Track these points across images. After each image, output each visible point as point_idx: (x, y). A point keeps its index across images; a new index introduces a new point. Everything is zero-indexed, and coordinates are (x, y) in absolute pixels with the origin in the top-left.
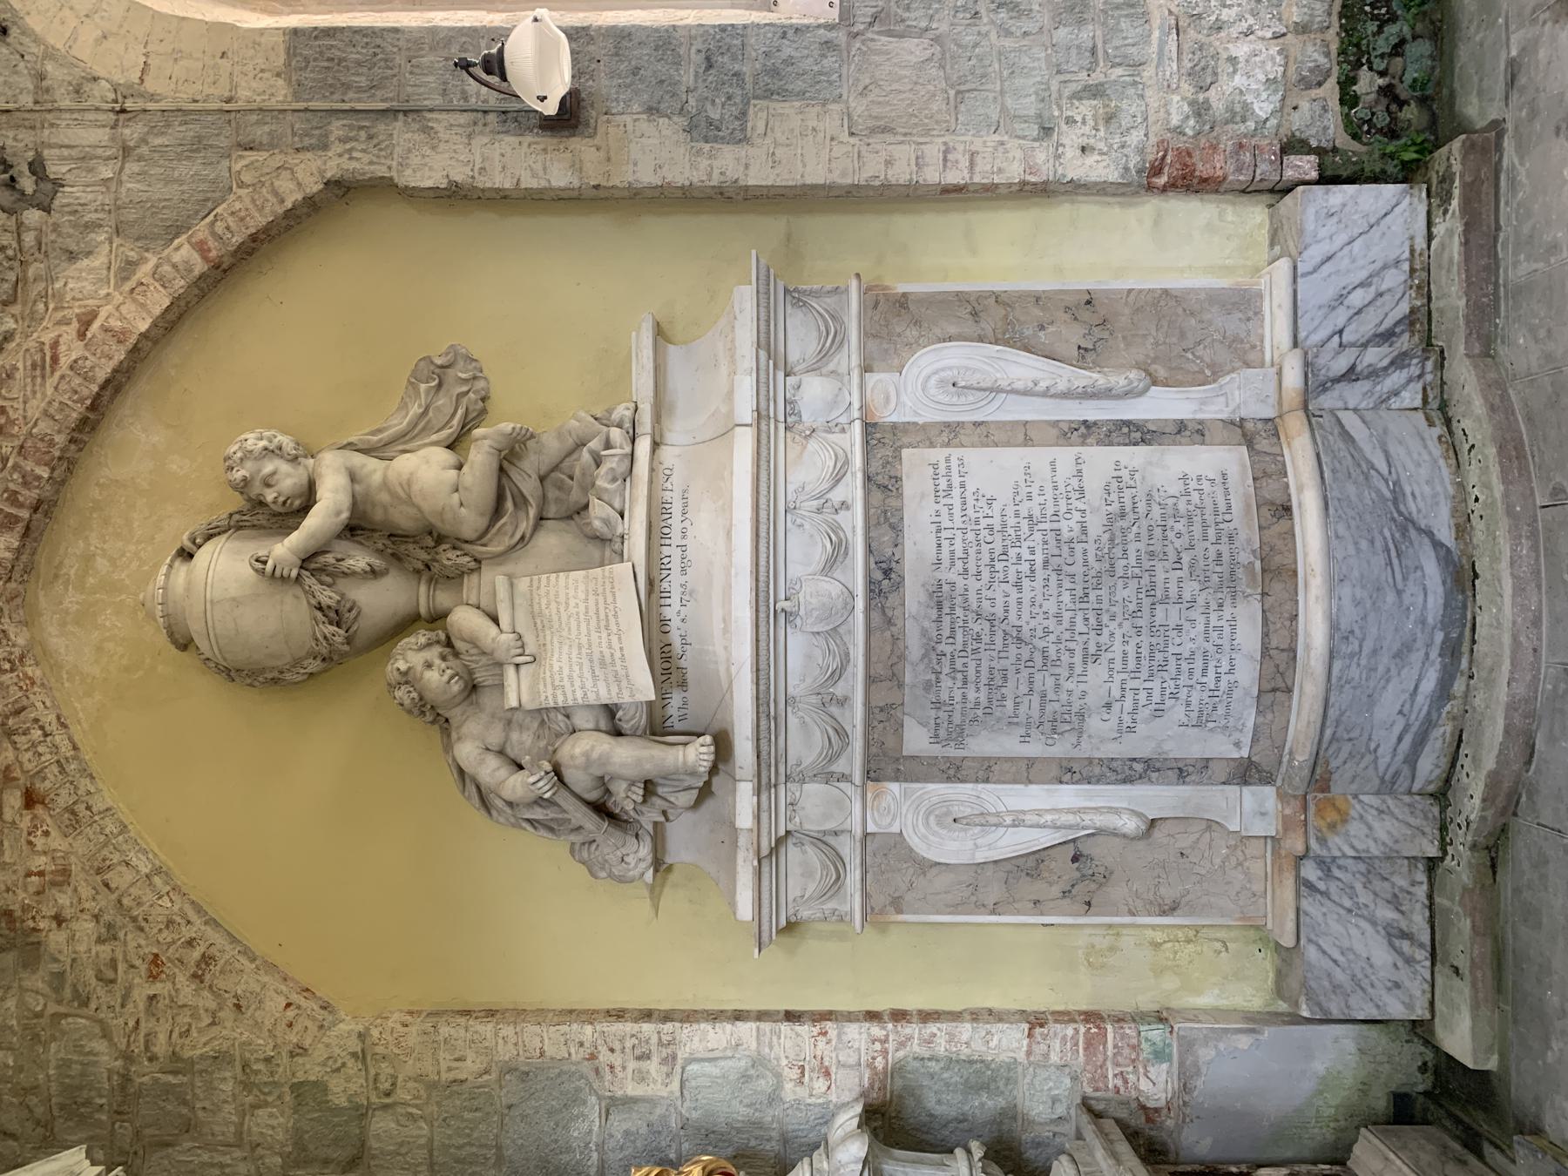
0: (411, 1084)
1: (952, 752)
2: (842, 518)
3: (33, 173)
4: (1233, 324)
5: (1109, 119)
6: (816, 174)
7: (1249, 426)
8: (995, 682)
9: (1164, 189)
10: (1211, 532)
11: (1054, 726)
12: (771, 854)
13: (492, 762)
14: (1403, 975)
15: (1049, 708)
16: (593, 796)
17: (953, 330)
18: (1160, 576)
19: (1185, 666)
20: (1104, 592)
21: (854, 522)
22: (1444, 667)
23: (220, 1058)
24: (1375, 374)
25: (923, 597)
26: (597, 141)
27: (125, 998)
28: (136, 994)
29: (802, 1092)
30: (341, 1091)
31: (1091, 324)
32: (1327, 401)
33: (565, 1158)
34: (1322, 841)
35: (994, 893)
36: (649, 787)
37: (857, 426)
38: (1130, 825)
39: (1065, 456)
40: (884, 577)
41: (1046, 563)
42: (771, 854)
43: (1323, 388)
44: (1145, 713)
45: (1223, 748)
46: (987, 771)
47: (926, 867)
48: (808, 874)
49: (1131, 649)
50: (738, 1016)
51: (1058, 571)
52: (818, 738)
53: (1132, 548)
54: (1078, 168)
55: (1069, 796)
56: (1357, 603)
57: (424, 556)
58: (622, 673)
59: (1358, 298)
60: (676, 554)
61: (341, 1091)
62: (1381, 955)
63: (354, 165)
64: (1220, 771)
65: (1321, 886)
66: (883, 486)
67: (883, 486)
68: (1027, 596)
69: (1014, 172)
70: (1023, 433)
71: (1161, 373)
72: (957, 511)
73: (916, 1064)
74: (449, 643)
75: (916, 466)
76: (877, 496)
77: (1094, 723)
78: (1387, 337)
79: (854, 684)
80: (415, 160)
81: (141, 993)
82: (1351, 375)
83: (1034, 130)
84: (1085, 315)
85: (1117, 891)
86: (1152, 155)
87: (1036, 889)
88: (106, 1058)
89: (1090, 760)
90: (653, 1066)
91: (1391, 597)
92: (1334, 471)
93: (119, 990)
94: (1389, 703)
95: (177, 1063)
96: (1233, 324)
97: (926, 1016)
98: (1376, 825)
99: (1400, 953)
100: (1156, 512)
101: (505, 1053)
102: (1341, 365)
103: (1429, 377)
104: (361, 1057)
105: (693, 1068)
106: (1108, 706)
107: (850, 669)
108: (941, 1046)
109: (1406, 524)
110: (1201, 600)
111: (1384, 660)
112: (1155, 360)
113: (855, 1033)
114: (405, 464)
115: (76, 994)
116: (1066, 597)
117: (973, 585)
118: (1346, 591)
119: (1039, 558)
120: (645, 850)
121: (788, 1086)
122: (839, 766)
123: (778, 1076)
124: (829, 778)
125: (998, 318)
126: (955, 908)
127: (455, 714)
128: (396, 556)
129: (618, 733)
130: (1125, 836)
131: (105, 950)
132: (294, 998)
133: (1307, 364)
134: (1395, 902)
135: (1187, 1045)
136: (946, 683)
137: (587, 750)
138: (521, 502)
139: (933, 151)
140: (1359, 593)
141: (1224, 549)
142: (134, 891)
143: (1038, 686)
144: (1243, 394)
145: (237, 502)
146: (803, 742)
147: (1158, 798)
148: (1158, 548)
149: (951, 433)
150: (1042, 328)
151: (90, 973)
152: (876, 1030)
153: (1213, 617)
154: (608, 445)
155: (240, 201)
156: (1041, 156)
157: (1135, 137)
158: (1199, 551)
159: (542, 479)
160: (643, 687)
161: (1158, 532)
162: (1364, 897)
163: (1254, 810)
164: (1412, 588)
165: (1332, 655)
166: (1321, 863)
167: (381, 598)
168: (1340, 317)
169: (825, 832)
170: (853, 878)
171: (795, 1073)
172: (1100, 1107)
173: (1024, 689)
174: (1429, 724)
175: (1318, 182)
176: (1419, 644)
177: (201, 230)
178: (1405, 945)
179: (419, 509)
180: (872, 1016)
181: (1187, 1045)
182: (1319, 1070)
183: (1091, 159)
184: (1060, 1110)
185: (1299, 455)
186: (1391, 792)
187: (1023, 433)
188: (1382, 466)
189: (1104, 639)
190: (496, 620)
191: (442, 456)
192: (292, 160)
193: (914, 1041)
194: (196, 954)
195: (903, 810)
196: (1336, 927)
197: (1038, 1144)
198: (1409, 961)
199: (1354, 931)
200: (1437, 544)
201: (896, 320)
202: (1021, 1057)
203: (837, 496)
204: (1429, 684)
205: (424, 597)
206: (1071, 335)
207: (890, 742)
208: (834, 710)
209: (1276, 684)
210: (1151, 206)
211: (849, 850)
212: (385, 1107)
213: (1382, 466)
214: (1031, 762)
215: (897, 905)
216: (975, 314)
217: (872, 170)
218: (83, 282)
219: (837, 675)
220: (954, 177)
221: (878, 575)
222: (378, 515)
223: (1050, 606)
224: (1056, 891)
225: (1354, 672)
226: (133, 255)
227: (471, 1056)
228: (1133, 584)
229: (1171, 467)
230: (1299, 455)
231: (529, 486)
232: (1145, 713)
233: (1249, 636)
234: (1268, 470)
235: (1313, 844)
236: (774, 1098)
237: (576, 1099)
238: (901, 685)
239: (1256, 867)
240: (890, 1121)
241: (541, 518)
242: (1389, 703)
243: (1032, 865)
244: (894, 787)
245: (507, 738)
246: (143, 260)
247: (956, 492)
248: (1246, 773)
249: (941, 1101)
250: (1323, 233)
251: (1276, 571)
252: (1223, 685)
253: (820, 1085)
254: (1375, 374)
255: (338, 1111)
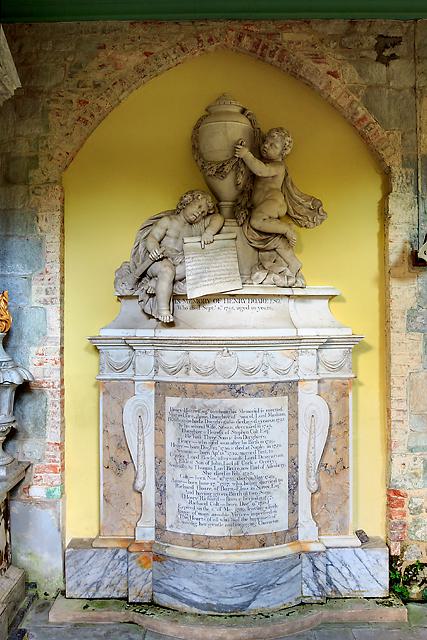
0: (36, 202)
1: (167, 416)
2: (261, 373)
3: (392, 55)
4: (335, 524)
5: (416, 474)
6: (395, 360)
7: (295, 531)
8: (196, 434)
9: (388, 496)
10: (255, 517)
11: (178, 456)
12: (126, 343)
13: (162, 232)
14: (82, 588)
15: (186, 455)
16: (149, 272)
17: (334, 416)
18: (238, 497)
19: (202, 506)
20: (231, 476)
21: (259, 377)
22: (203, 605)
23: (47, 128)
24: (316, 578)
25: (229, 406)
26: (407, 274)
27: (72, 92)
28: (74, 95)
29: (33, 354)
30: (34, 174)
31: (335, 468)
32: (305, 560)
33: (8, 262)
34: (134, 558)
35: (111, 430)
36: (152, 295)
37: (297, 378)
38: (139, 485)
39: (285, 460)
40: (236, 390)
41: (243, 454)
42: (126, 343)
43: (311, 559)
44: (183, 490)
45: (170, 520)
46: (160, 430)
47: (121, 404)
48: (118, 357)
49: (209, 486)
50: (62, 329)
51: (240, 458)
52: (172, 363)
53: (249, 486)
54: (397, 461)
55: (150, 461)
56: (227, 573)
57: (243, 203)
58: (198, 285)
59: (345, 571)
60: (245, 305)
61: (34, 174)
62: (90, 580)
63: (397, 177)
64: (160, 519)
65: (116, 557)
66: (274, 389)
67: (274, 389)
68: (230, 446)
69: (395, 438)
70: (293, 444)
71: (316, 496)
72: (264, 419)
73: (44, 399)
74: (209, 214)
75: (280, 402)
76: (269, 386)
77: (179, 471)
78: (330, 582)
79: (194, 377)
80: (399, 201)
81: (74, 97)
82: (315, 569)
83: (412, 445)
84: (340, 466)
85: (113, 478)
86: (402, 491)
87: (113, 444)
88: (48, 85)
89: (165, 469)
90: (43, 296)
91: (230, 585)
92: (278, 563)
93: (76, 89)
94: (189, 584)
95: (45, 112)
96: (335, 524)
97: (62, 403)
98: (141, 578)
99: (91, 586)
100: (263, 496)
101: (48, 238)
102: (319, 565)
103: (314, 598)
104: (48, 182)
105: (42, 312)
106: (186, 477)
107: (200, 376)
108: (51, 409)
109: (257, 590)
110: (228, 513)
111: (205, 583)
112: (322, 494)
113: (56, 376)
114: (281, 199)
115: (73, 73)
116: (229, 461)
117: (234, 425)
118: (232, 568)
119: (244, 451)
120: (127, 292)
121: (36, 349)
122: (160, 371)
123: (39, 345)
124: (156, 367)
125: (339, 426)
126: (105, 416)
127: (181, 217)
128: (242, 192)
129: (174, 282)
130: (135, 482)
131: (90, 83)
132: (71, 155)
133: (320, 553)
134: (110, 585)
135: (53, 505)
136: (195, 415)
137: (164, 271)
138: (265, 241)
139: (403, 406)
140: (232, 573)
141: (249, 521)
142: (112, 95)
143: (194, 450)
144: (307, 530)
145: (265, 130)
146: (171, 357)
147: (150, 495)
148: (249, 496)
149: (294, 415)
150: (335, 450)
151: (81, 78)
152: (57, 384)
153: (222, 518)
154: (288, 278)
155: (383, 134)
156: (402, 449)
157: (408, 485)
158: (249, 512)
159: (275, 250)
160: (194, 293)
161: (255, 497)
162: (112, 574)
163: (146, 533)
164: (234, 593)
165: (207, 563)
166: (124, 558)
167: (227, 187)
168: (338, 565)
169: (134, 364)
170: (117, 375)
171: (40, 352)
172: (29, 470)
173: (193, 445)
174: (180, 599)
175: (390, 555)
176: (211, 596)
177: (371, 118)
178: (94, 589)
179: (262, 203)
180: (62, 381)
181: (53, 505)
182: (42, 560)
183: (401, 468)
184: (28, 455)
185: (285, 550)
186: (153, 584)
187: (293, 444)
188: (282, 580)
189: (213, 476)
190: (218, 233)
191: (283, 212)
192: (399, 154)
193: (51, 397)
194: (88, 118)
195: (145, 397)
196: (100, 562)
197: (14, 447)
198: (88, 589)
199: (98, 569)
200: (250, 602)
201: (340, 393)
202: (48, 440)
203: (270, 371)
204: (196, 599)
205: (226, 206)
206: (331, 460)
207: (170, 392)
208: (184, 369)
209: (195, 542)
210: (383, 492)
211: (129, 373)
212: (28, 192)
213: (282, 580)
214: (163, 446)
215: (106, 393)
216: (340, 423)
217: (396, 382)
218: (350, 72)
219: (198, 371)
220: (394, 414)
221: (238, 387)
222: (259, 186)
223: (225, 455)
224: (112, 454)
225: (201, 571)
226: (360, 93)
227: (48, 225)
228: (234, 487)
229: (280, 499)
230: (285, 550)
231: (272, 244)
232: (183, 490)
233: (214, 532)
234: (278, 538)
235: (133, 555)
236: (31, 343)
237: (31, 266)
238: (194, 397)
239: (123, 533)
240: (23, 390)
241: (258, 250)
242: (189, 584)
243: (123, 446)
244: (153, 392)
245: (170, 237)
246: (358, 97)
247: (271, 418)
248: (160, 528)
249: (29, 407)
250: (370, 558)
251: (241, 541)
252: (195, 521)
253: (36, 362)
254: (316, 578)
255: (28, 173)
